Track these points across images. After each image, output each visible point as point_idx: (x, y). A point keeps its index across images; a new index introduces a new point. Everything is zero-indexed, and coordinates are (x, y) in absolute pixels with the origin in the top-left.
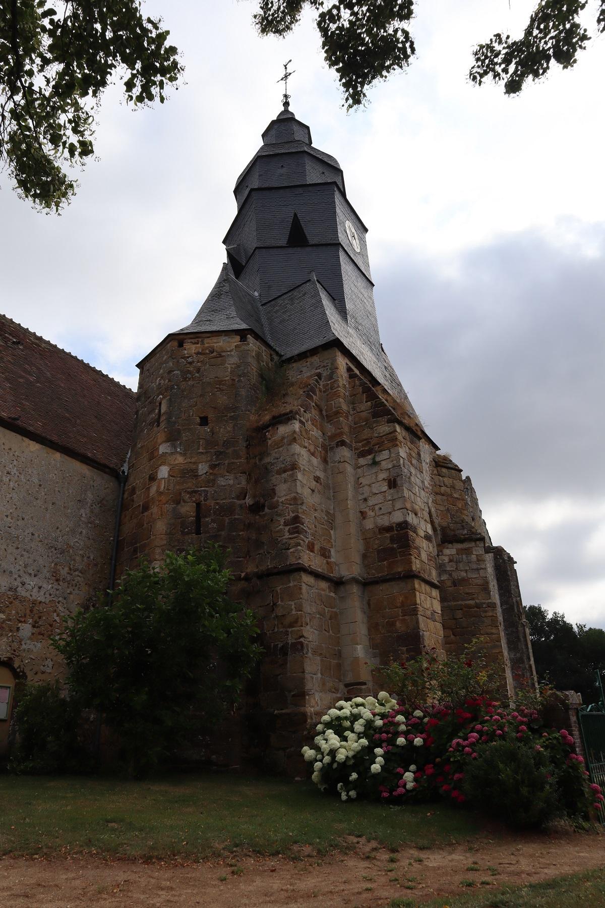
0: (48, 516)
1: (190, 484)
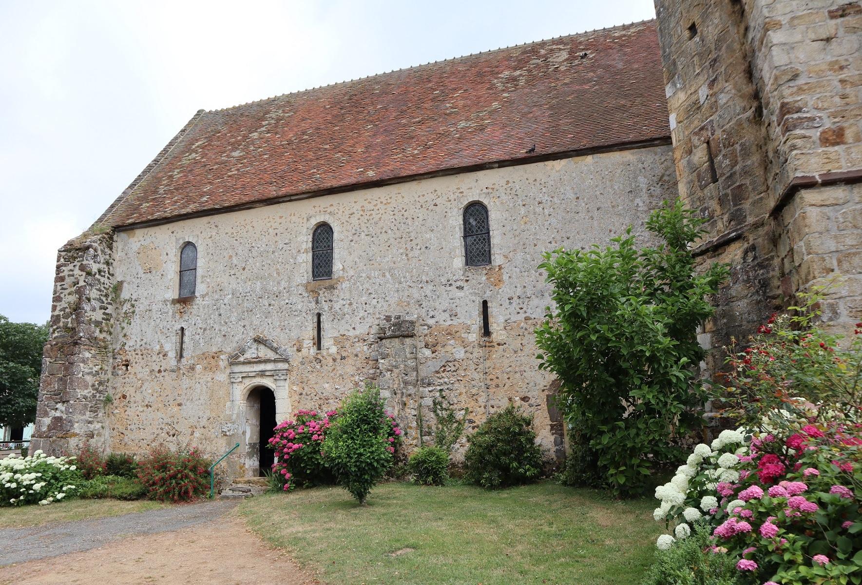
0: (595, 223)
1: (696, 122)
